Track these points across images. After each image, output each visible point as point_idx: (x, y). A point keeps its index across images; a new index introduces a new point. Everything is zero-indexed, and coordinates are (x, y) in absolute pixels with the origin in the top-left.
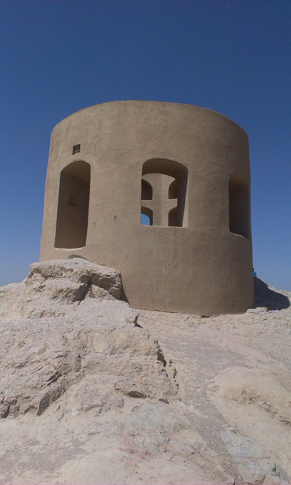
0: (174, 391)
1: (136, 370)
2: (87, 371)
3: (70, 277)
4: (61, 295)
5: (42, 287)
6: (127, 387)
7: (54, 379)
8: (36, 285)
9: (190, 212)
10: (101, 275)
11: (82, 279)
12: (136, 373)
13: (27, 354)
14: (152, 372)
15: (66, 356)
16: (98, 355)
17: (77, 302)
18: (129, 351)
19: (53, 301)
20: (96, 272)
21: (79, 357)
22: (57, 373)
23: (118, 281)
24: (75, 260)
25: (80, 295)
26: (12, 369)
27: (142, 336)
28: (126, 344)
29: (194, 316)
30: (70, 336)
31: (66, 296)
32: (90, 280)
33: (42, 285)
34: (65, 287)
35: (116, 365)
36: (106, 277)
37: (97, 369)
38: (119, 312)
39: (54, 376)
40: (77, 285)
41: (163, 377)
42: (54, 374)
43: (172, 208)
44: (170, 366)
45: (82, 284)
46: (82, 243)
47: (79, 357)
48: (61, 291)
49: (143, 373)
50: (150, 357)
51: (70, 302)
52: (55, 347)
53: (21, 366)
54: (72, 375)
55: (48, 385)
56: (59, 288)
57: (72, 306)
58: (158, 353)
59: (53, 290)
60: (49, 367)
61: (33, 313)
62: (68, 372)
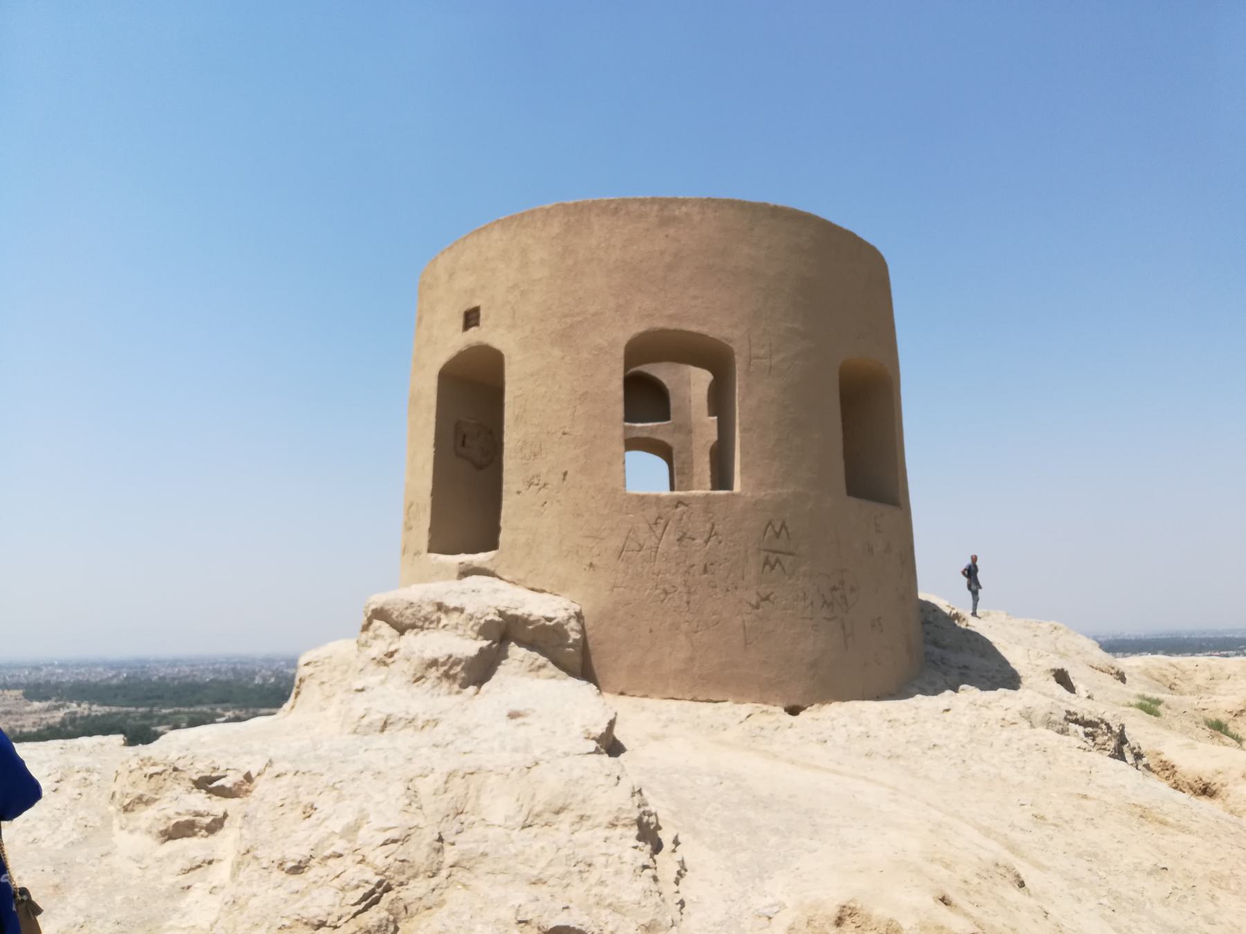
0: (669, 918)
1: (577, 869)
2: (459, 874)
3: (456, 627)
4: (434, 673)
5: (391, 655)
6: (546, 916)
7: (370, 900)
8: (378, 649)
9: (744, 453)
10: (532, 619)
11: (485, 630)
12: (576, 877)
13: (313, 840)
14: (617, 873)
15: (405, 839)
16: (491, 832)
17: (472, 689)
18: (567, 818)
19: (415, 689)
20: (519, 612)
21: (440, 839)
22: (379, 884)
23: (572, 630)
24: (473, 581)
25: (479, 671)
26: (278, 875)
27: (601, 780)
28: (560, 804)
29: (765, 707)
30: (425, 787)
31: (446, 675)
32: (506, 632)
33: (392, 648)
34: (441, 655)
35: (528, 860)
36: (543, 621)
37: (483, 868)
38: (576, 705)
39: (373, 892)
40: (471, 647)
41: (645, 880)
42: (372, 887)
43: (27, 814)
44: (674, 851)
45: (485, 643)
46: (490, 542)
47: (440, 839)
48: (434, 663)
49: (593, 877)
50: (619, 831)
51: (456, 687)
52: (386, 812)
53: (298, 869)
54: (418, 888)
55: (354, 916)
56: (429, 655)
57: (459, 698)
58: (639, 822)
59: (415, 662)
60: (362, 870)
61: (365, 721)
62: (408, 879)
